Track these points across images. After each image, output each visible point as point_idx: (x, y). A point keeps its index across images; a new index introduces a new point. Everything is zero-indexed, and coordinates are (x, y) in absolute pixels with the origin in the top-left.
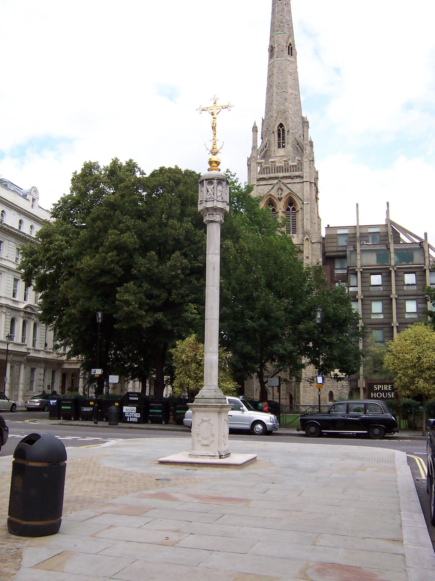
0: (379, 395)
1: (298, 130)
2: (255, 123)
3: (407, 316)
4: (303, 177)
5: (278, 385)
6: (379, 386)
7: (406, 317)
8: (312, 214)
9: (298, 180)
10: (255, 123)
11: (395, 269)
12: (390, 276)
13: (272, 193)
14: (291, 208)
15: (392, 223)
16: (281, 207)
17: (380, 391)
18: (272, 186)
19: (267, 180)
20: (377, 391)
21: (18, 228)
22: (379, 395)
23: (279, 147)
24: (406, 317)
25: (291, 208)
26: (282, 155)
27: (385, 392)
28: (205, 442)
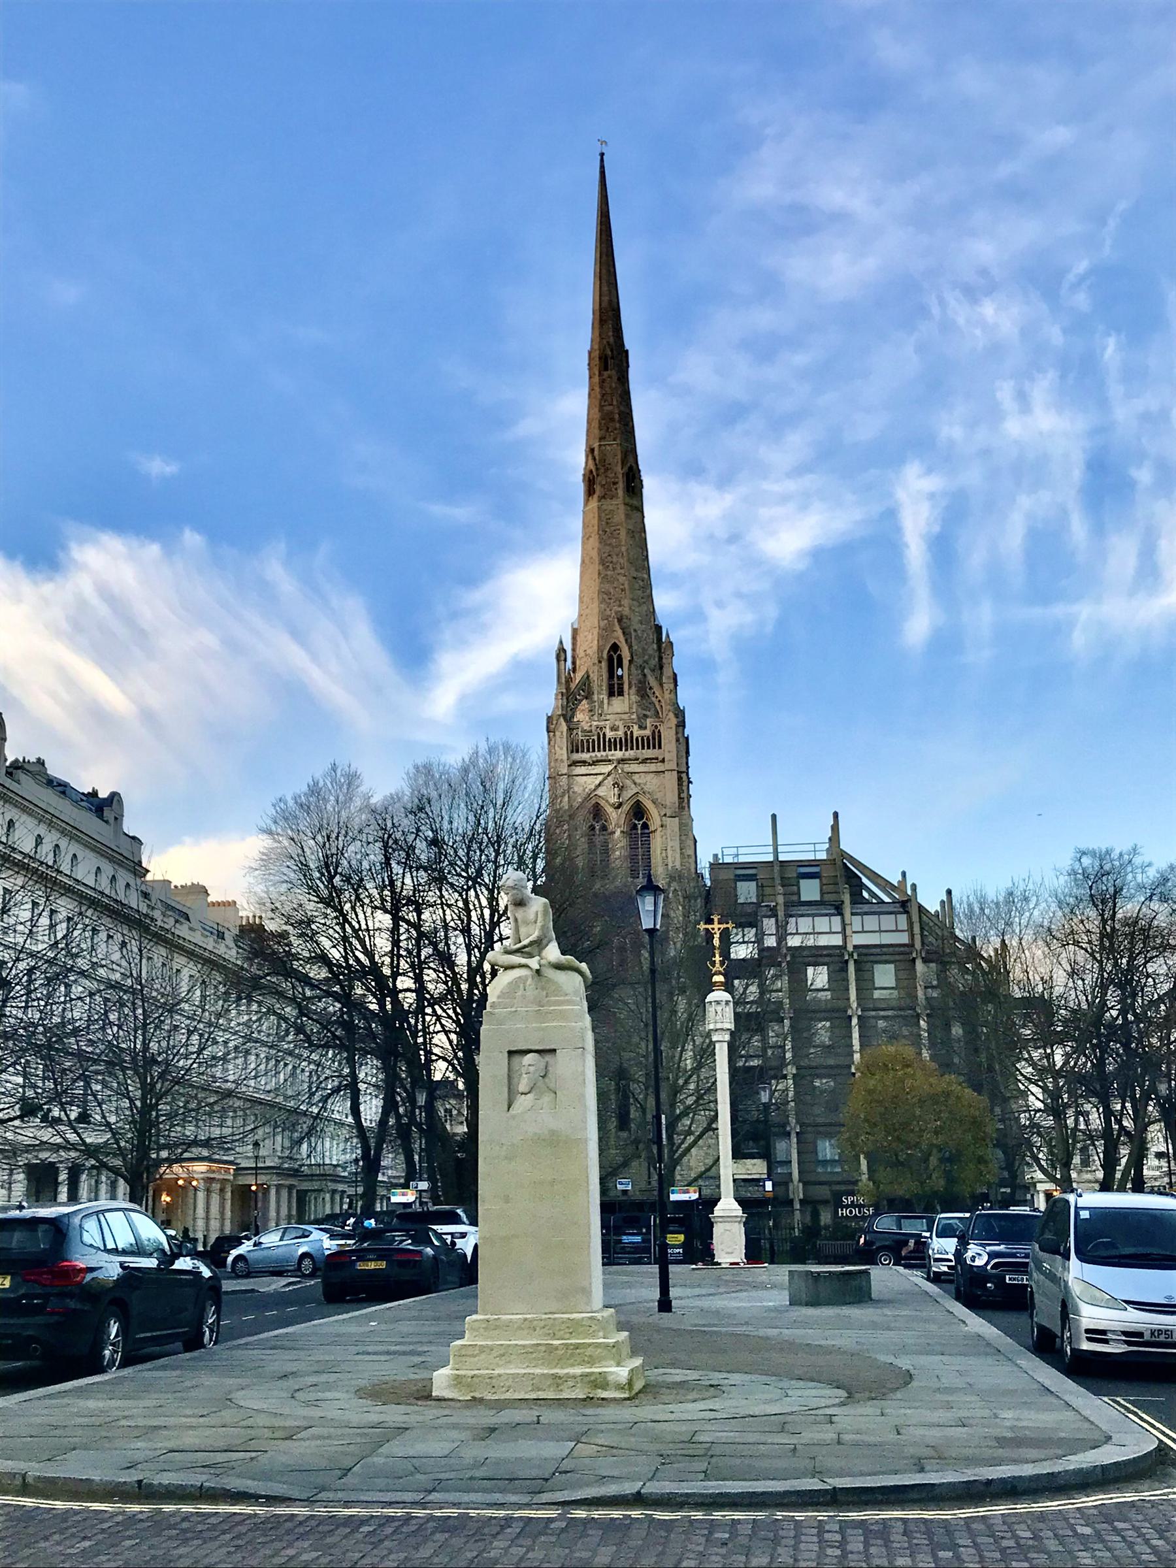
0: (851, 1212)
1: (650, 656)
2: (561, 642)
3: (877, 994)
4: (663, 761)
5: (965, 1190)
6: (850, 1199)
7: (875, 996)
8: (683, 838)
9: (653, 767)
10: (561, 642)
11: (855, 957)
12: (844, 969)
13: (601, 792)
14: (639, 824)
15: (844, 855)
16: (616, 819)
17: (853, 1205)
18: (600, 778)
19: (590, 765)
20: (847, 1206)
21: (92, 884)
22: (851, 1212)
23: (611, 694)
24: (875, 996)
25: (639, 824)
26: (619, 711)
27: (860, 1206)
28: (729, 1250)
